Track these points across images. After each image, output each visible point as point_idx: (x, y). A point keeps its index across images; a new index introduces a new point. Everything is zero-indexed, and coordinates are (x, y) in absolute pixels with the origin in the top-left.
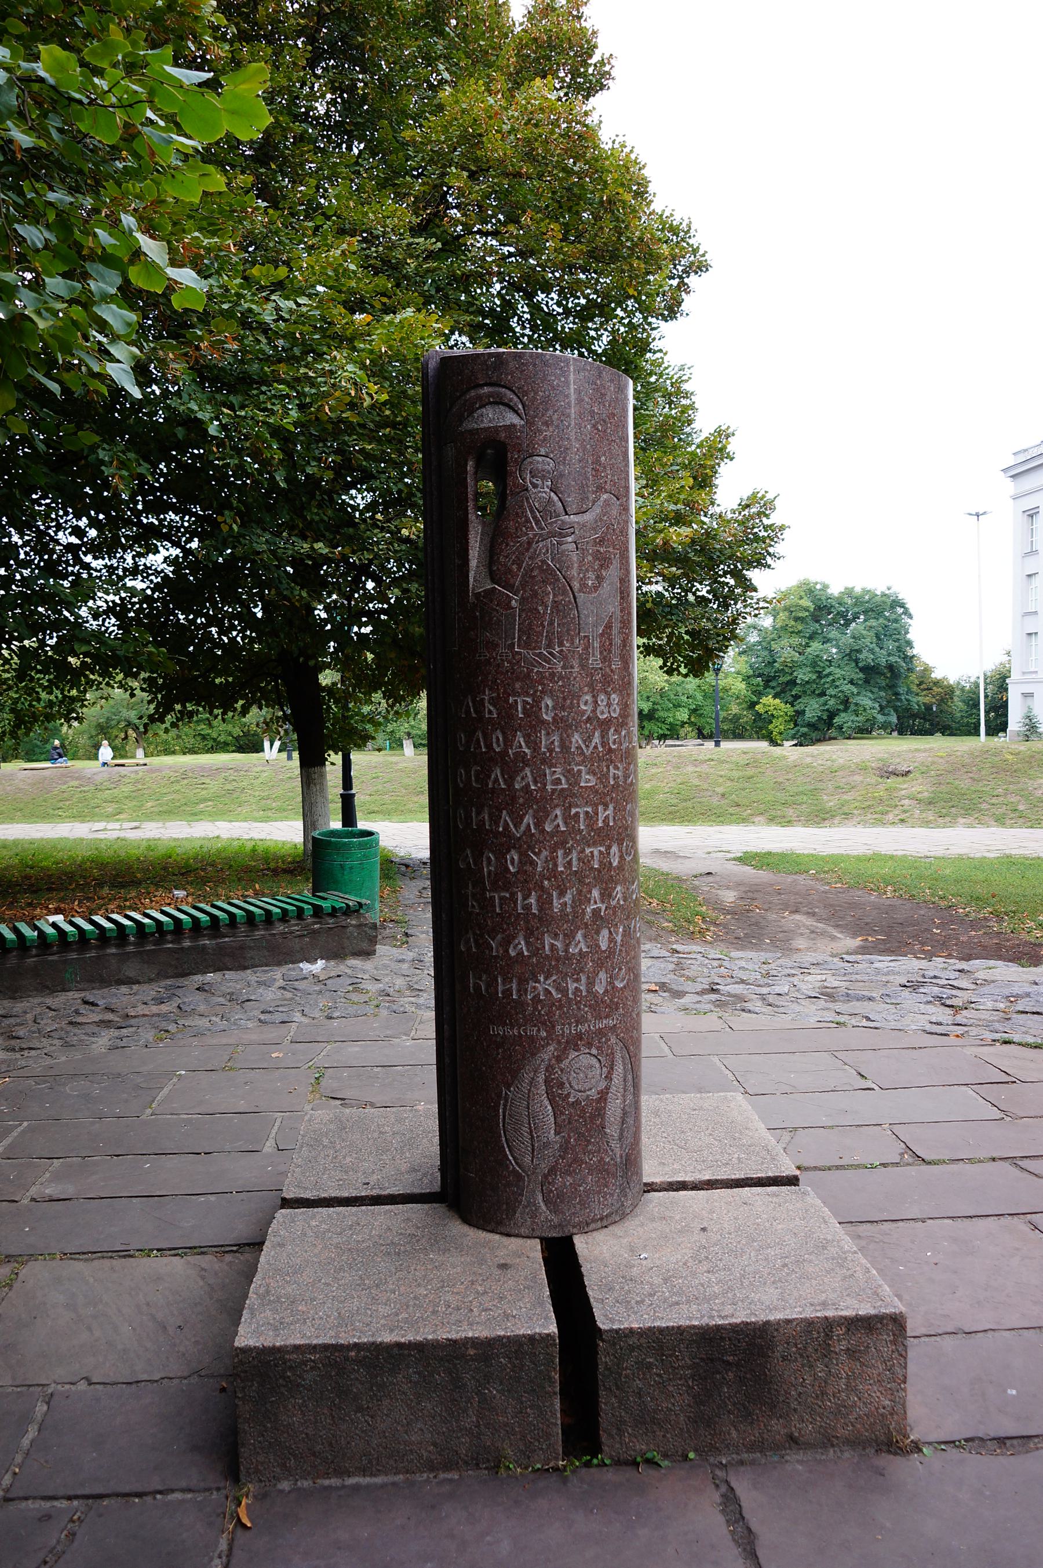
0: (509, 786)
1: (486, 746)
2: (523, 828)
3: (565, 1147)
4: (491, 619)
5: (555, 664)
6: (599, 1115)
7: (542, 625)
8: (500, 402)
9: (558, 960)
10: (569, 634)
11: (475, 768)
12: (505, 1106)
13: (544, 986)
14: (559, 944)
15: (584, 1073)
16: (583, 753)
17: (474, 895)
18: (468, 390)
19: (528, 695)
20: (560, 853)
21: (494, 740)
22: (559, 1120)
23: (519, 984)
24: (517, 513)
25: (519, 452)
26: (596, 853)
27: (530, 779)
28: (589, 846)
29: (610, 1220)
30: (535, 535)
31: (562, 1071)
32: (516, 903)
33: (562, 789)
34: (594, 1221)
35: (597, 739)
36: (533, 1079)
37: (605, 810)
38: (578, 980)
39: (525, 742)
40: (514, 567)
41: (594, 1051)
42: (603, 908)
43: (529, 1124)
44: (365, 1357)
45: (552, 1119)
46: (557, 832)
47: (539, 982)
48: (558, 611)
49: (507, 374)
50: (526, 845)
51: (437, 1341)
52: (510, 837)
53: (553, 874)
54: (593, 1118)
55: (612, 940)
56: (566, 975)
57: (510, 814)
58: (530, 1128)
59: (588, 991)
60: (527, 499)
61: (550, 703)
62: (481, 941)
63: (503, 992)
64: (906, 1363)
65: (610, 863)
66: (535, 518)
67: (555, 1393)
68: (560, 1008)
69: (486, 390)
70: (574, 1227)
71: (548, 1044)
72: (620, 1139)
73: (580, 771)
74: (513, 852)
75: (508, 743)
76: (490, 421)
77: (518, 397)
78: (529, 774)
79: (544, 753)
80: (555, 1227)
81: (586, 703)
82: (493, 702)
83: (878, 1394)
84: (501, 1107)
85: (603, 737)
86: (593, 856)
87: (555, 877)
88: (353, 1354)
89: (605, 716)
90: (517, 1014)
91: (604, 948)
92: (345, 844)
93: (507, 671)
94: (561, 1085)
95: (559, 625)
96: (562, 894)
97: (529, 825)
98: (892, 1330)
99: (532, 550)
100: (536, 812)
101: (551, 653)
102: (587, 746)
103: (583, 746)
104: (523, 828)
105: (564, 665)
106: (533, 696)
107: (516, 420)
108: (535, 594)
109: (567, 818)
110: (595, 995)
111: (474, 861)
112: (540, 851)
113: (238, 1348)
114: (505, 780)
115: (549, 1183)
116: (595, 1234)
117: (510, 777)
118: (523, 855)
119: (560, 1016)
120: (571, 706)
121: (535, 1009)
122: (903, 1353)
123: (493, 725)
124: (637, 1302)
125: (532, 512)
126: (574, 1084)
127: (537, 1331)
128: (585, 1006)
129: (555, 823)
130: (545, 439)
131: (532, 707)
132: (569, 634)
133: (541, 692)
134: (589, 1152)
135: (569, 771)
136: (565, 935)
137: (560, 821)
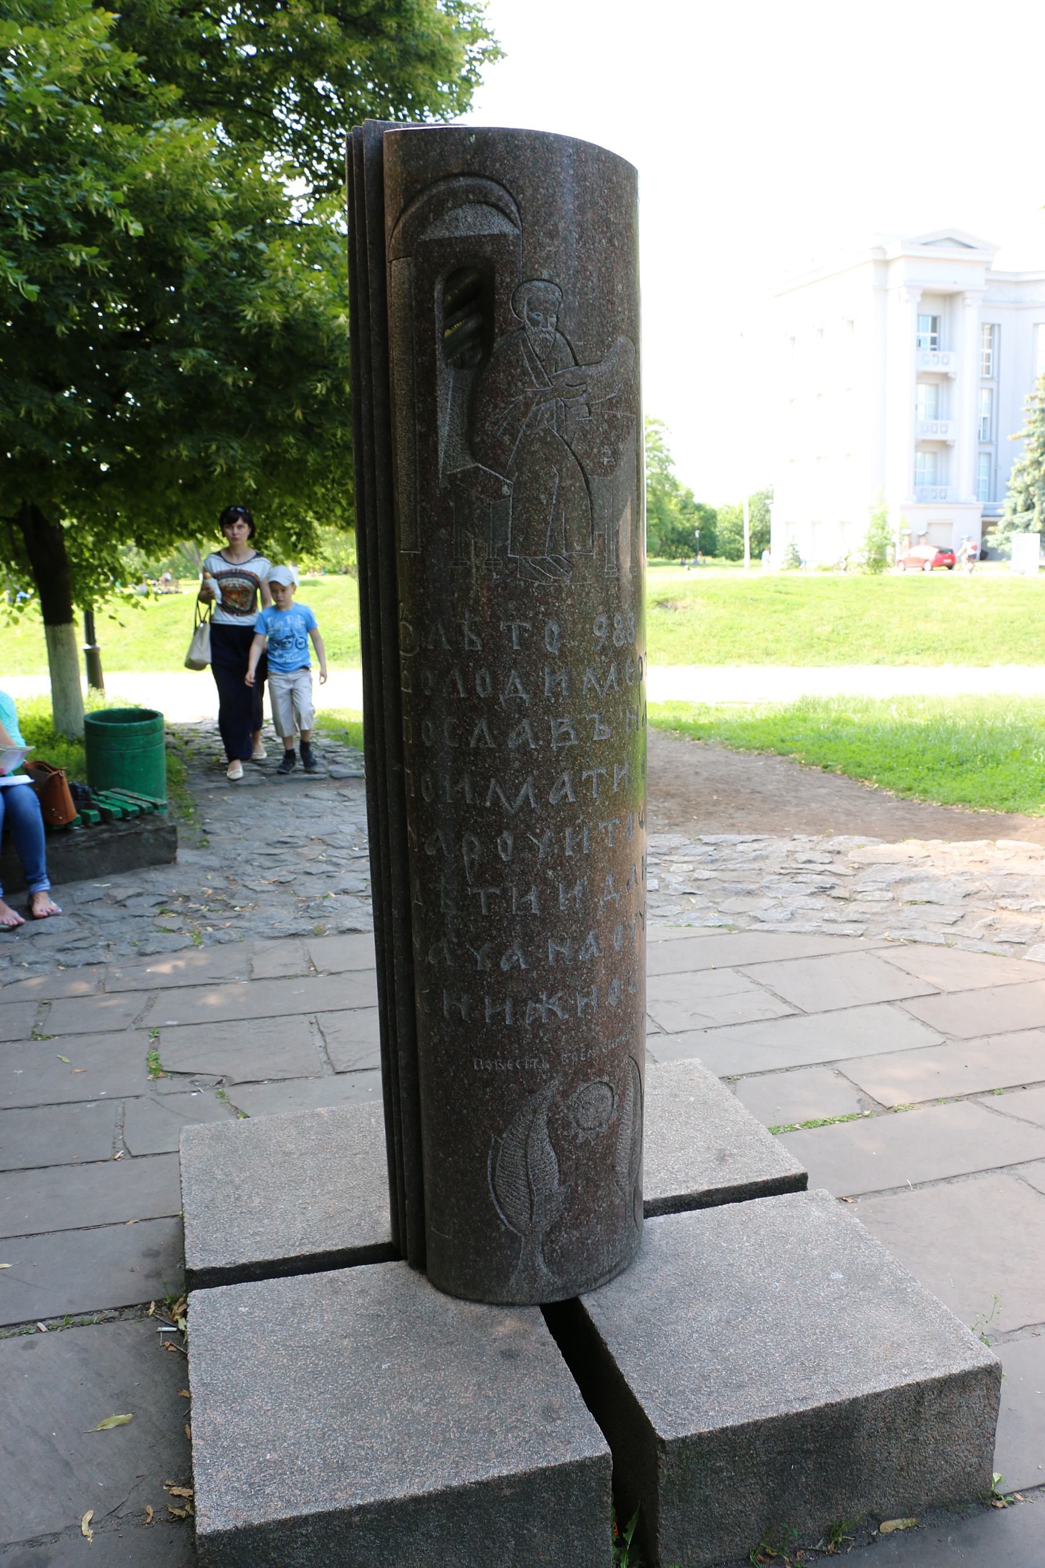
1: (466, 690)
3: (572, 1198)
7: (545, 520)
8: (484, 200)
9: (564, 972)
10: (580, 533)
12: (495, 1157)
16: (596, 697)
19: (526, 618)
21: (478, 682)
22: (565, 1167)
23: (514, 1005)
24: (510, 362)
25: (512, 273)
26: (610, 828)
29: (618, 1269)
30: (535, 394)
31: (568, 1108)
32: (509, 901)
33: (571, 747)
34: (602, 1275)
36: (532, 1122)
37: (621, 769)
39: (522, 683)
40: (506, 438)
43: (527, 1175)
44: (372, 1521)
46: (565, 804)
51: (464, 1486)
52: (500, 814)
53: (559, 861)
57: (501, 783)
60: (524, 341)
61: (555, 629)
62: (459, 952)
63: (492, 1017)
64: (997, 1416)
66: (534, 368)
67: (607, 1519)
69: (462, 181)
70: (580, 1286)
71: (552, 1077)
73: (593, 720)
74: (505, 834)
75: (497, 685)
76: (469, 228)
77: (511, 194)
80: (558, 1290)
81: (600, 627)
82: (475, 628)
83: (966, 1453)
84: (490, 1157)
87: (561, 864)
88: (357, 1519)
89: (622, 643)
90: (511, 1043)
92: (125, 728)
93: (497, 586)
94: (567, 1125)
95: (567, 520)
96: (570, 885)
97: (527, 798)
98: (987, 1384)
99: (530, 414)
102: (601, 686)
103: (597, 687)
106: (534, 619)
107: (507, 228)
108: (536, 477)
112: (542, 831)
113: (201, 1537)
115: (552, 1242)
118: (520, 838)
119: (567, 1041)
121: (536, 1036)
122: (996, 1406)
123: (476, 661)
124: (692, 1391)
125: (531, 360)
126: (581, 1122)
127: (587, 1454)
128: (596, 1024)
129: (562, 792)
130: (548, 257)
131: (531, 636)
135: (579, 722)
136: (574, 939)
137: (568, 789)
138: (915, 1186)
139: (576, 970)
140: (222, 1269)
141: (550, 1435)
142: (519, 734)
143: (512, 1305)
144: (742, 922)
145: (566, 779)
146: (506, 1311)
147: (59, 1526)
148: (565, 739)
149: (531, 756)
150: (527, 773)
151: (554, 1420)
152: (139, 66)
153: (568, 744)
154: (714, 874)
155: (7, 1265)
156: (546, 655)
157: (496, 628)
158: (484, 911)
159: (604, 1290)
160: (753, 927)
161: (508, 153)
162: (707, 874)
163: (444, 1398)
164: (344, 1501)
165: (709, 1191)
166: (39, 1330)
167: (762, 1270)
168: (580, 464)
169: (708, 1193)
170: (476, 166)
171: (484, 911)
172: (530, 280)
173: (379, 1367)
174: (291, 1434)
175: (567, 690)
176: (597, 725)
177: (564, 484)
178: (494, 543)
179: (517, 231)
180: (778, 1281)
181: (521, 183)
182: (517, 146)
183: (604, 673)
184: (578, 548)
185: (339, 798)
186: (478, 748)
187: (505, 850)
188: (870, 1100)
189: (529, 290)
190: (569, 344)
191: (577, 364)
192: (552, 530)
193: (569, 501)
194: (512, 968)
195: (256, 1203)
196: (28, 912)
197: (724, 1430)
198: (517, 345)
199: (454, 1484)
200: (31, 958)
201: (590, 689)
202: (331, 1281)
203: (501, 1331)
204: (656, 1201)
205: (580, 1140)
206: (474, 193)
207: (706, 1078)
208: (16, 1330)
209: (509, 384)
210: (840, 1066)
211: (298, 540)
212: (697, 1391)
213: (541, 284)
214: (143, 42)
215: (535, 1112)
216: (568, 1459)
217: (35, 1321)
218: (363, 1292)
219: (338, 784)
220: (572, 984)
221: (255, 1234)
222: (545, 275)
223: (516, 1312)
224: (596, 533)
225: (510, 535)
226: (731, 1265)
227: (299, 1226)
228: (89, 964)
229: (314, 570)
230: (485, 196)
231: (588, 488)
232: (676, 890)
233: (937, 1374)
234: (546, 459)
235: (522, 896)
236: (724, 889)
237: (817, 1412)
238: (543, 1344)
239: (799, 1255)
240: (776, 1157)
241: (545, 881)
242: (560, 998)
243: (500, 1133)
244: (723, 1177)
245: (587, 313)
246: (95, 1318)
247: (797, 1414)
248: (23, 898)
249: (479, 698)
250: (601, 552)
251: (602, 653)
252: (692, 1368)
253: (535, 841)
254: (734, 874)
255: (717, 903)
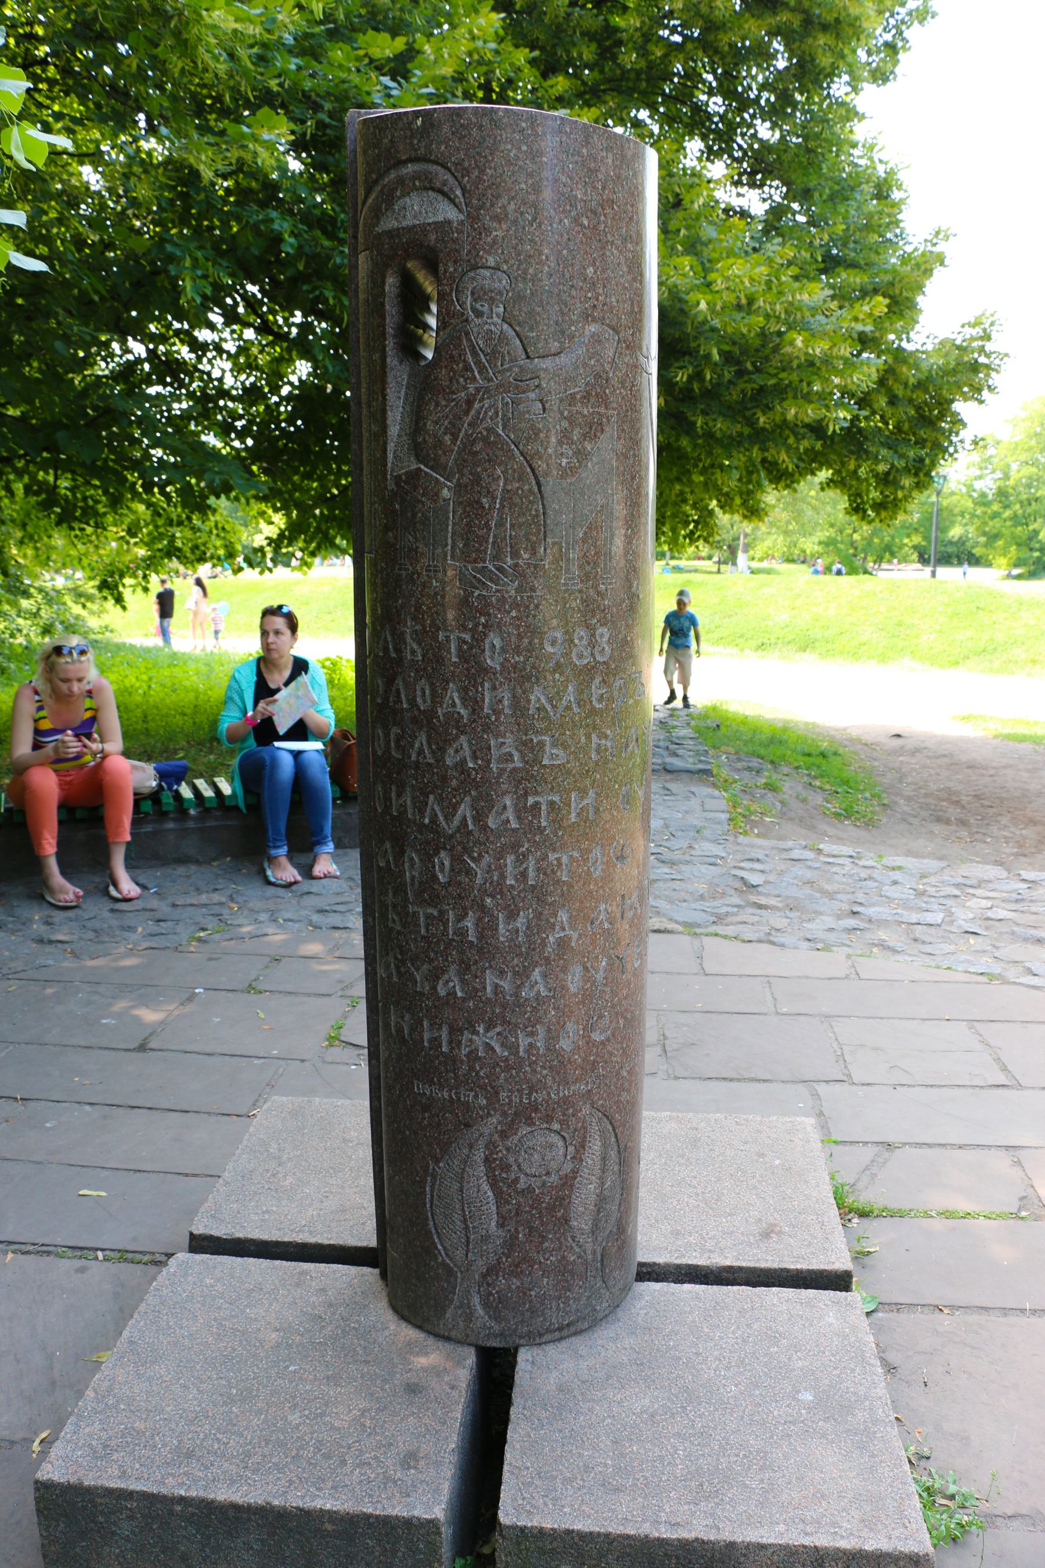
0: (438, 761)
2: (456, 821)
3: (511, 1243)
4: (414, 515)
5: (505, 584)
6: (561, 1205)
8: (429, 186)
9: (504, 1006)
10: (528, 540)
11: (395, 730)
13: (483, 1038)
14: (505, 985)
15: (541, 1152)
16: (547, 718)
17: (395, 906)
18: (388, 170)
20: (510, 859)
21: (419, 693)
23: (450, 1033)
24: (452, 357)
26: (565, 860)
27: (467, 752)
28: (554, 850)
29: (572, 1329)
30: (478, 390)
31: (508, 1149)
33: (515, 769)
34: (548, 1331)
35: (570, 694)
37: (582, 798)
38: (532, 1034)
41: (556, 1126)
42: (575, 936)
43: (463, 1210)
44: (193, 1514)
45: (494, 1208)
46: (506, 830)
47: (477, 1033)
48: (512, 505)
49: (439, 143)
50: (462, 845)
51: (284, 1508)
52: (438, 832)
53: (499, 889)
54: (551, 1209)
55: (587, 978)
56: (516, 1025)
57: (440, 800)
58: (464, 1216)
59: (548, 1049)
60: (467, 334)
61: (497, 642)
63: (430, 1041)
65: (589, 873)
66: (478, 363)
68: (508, 1068)
69: (410, 168)
70: (520, 1337)
71: (489, 1115)
72: (593, 1232)
74: (443, 854)
75: (437, 698)
76: (415, 217)
78: (465, 745)
79: (488, 717)
80: (496, 1336)
81: (553, 643)
85: (580, 692)
86: (560, 865)
87: (501, 892)
88: (179, 1508)
89: (586, 661)
91: (573, 989)
95: (512, 526)
96: (512, 916)
97: (465, 819)
99: (473, 412)
100: (474, 800)
101: (500, 569)
102: (554, 707)
104: (456, 821)
105: (520, 586)
106: (473, 630)
108: (477, 480)
109: (521, 811)
110: (559, 1054)
111: (395, 859)
114: (433, 752)
115: (489, 1285)
116: (551, 1346)
117: (440, 749)
118: (457, 860)
119: (506, 1080)
120: (530, 649)
121: (471, 1068)
123: (417, 671)
125: (474, 354)
126: (524, 1166)
127: (416, 1513)
128: (543, 1067)
129: (504, 817)
130: (495, 242)
131: (471, 648)
132: (528, 540)
133: (484, 626)
134: (545, 1251)
135: (524, 744)
136: (516, 974)
137: (510, 814)
138: (1034, 1312)
139: (519, 1006)
140: (218, 1239)
141: (395, 1482)
142: (457, 751)
143: (448, 1339)
144: (1011, 974)
145: (508, 803)
146: (440, 1344)
147: (19, 1436)
148: (507, 761)
149: (469, 775)
150: (465, 793)
151: (409, 1468)
152: (532, 62)
153: (511, 766)
154: (1011, 915)
155: (103, 1194)
156: (485, 669)
157: (435, 638)
158: (423, 931)
159: (551, 1350)
160: (1022, 980)
161: (453, 133)
162: (1002, 914)
163: (323, 1414)
164: (175, 1486)
165: (731, 1268)
166: (96, 1258)
167: (728, 1368)
168: (530, 466)
169: (730, 1269)
170: (422, 151)
171: (423, 931)
172: (475, 267)
173: (287, 1367)
174: (168, 1409)
175: (509, 707)
176: (547, 748)
177: (509, 487)
178: (435, 549)
179: (461, 217)
180: (736, 1386)
181: (466, 164)
182: (462, 125)
183: (558, 693)
184: (526, 556)
185: (662, 792)
186: (418, 761)
187: (442, 871)
188: (1036, 1201)
189: (473, 279)
190: (518, 335)
191: (528, 357)
192: (495, 536)
193: (515, 505)
194: (448, 994)
195: (287, 1183)
196: (307, 872)
197: (569, 1532)
198: (459, 338)
199: (276, 1503)
200: (288, 916)
201: (538, 709)
202: (303, 1273)
203: (423, 1361)
204: (668, 1265)
205: (522, 1185)
206: (419, 179)
207: (808, 1141)
208: (79, 1253)
209: (451, 381)
210: (1023, 1154)
211: (696, 527)
212: (566, 1481)
213: (487, 273)
214: (542, 37)
215: (471, 1147)
216: (394, 1513)
217: (97, 1249)
218: (323, 1290)
219: (669, 777)
220: (513, 1021)
221: (267, 1212)
222: (491, 261)
223: (449, 1347)
224: (549, 540)
225: (450, 541)
226: (698, 1354)
227: (311, 1212)
228: (335, 928)
229: (773, 557)
230: (430, 182)
231: (540, 491)
232: (960, 927)
233: (844, 1544)
234: (489, 461)
235: (459, 921)
236: (1013, 933)
237: (685, 1545)
238: (452, 1388)
239: (779, 1362)
240: (827, 1245)
241: (482, 908)
242: (499, 1034)
243: (437, 1161)
244: (754, 1255)
245: (541, 301)
246: (146, 1258)
247: (658, 1539)
248: (304, 859)
249: (419, 709)
250: (556, 561)
251: (555, 671)
252: (580, 1455)
253: (472, 865)
254: (1034, 917)
255: (997, 948)
